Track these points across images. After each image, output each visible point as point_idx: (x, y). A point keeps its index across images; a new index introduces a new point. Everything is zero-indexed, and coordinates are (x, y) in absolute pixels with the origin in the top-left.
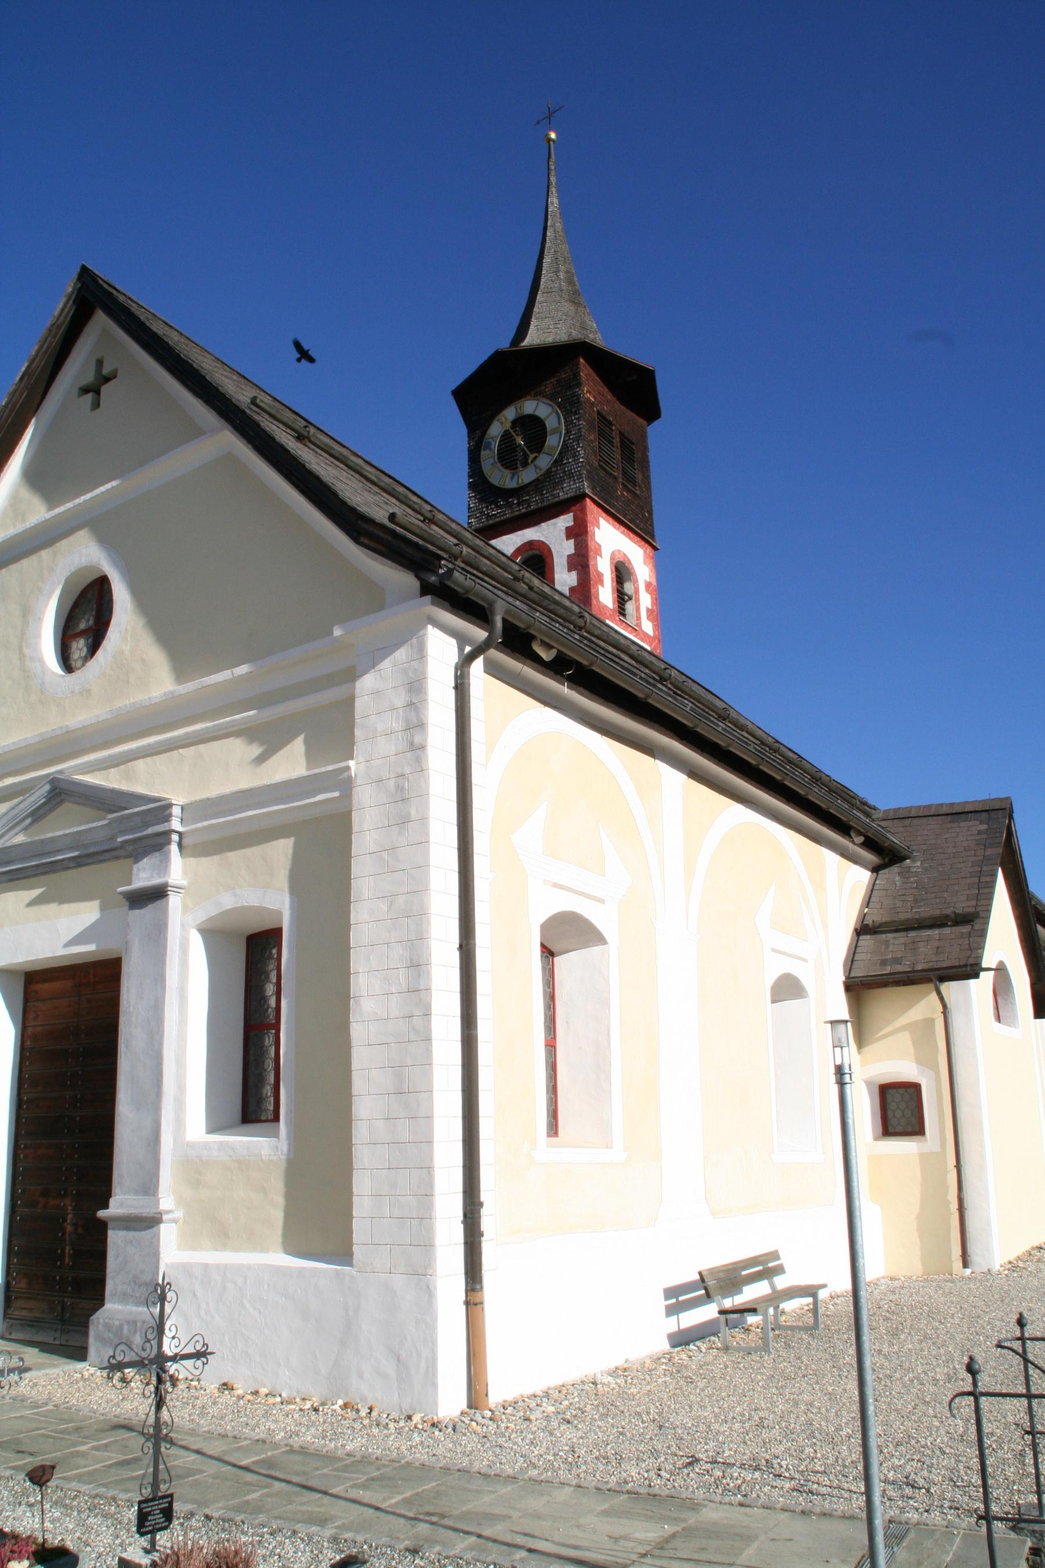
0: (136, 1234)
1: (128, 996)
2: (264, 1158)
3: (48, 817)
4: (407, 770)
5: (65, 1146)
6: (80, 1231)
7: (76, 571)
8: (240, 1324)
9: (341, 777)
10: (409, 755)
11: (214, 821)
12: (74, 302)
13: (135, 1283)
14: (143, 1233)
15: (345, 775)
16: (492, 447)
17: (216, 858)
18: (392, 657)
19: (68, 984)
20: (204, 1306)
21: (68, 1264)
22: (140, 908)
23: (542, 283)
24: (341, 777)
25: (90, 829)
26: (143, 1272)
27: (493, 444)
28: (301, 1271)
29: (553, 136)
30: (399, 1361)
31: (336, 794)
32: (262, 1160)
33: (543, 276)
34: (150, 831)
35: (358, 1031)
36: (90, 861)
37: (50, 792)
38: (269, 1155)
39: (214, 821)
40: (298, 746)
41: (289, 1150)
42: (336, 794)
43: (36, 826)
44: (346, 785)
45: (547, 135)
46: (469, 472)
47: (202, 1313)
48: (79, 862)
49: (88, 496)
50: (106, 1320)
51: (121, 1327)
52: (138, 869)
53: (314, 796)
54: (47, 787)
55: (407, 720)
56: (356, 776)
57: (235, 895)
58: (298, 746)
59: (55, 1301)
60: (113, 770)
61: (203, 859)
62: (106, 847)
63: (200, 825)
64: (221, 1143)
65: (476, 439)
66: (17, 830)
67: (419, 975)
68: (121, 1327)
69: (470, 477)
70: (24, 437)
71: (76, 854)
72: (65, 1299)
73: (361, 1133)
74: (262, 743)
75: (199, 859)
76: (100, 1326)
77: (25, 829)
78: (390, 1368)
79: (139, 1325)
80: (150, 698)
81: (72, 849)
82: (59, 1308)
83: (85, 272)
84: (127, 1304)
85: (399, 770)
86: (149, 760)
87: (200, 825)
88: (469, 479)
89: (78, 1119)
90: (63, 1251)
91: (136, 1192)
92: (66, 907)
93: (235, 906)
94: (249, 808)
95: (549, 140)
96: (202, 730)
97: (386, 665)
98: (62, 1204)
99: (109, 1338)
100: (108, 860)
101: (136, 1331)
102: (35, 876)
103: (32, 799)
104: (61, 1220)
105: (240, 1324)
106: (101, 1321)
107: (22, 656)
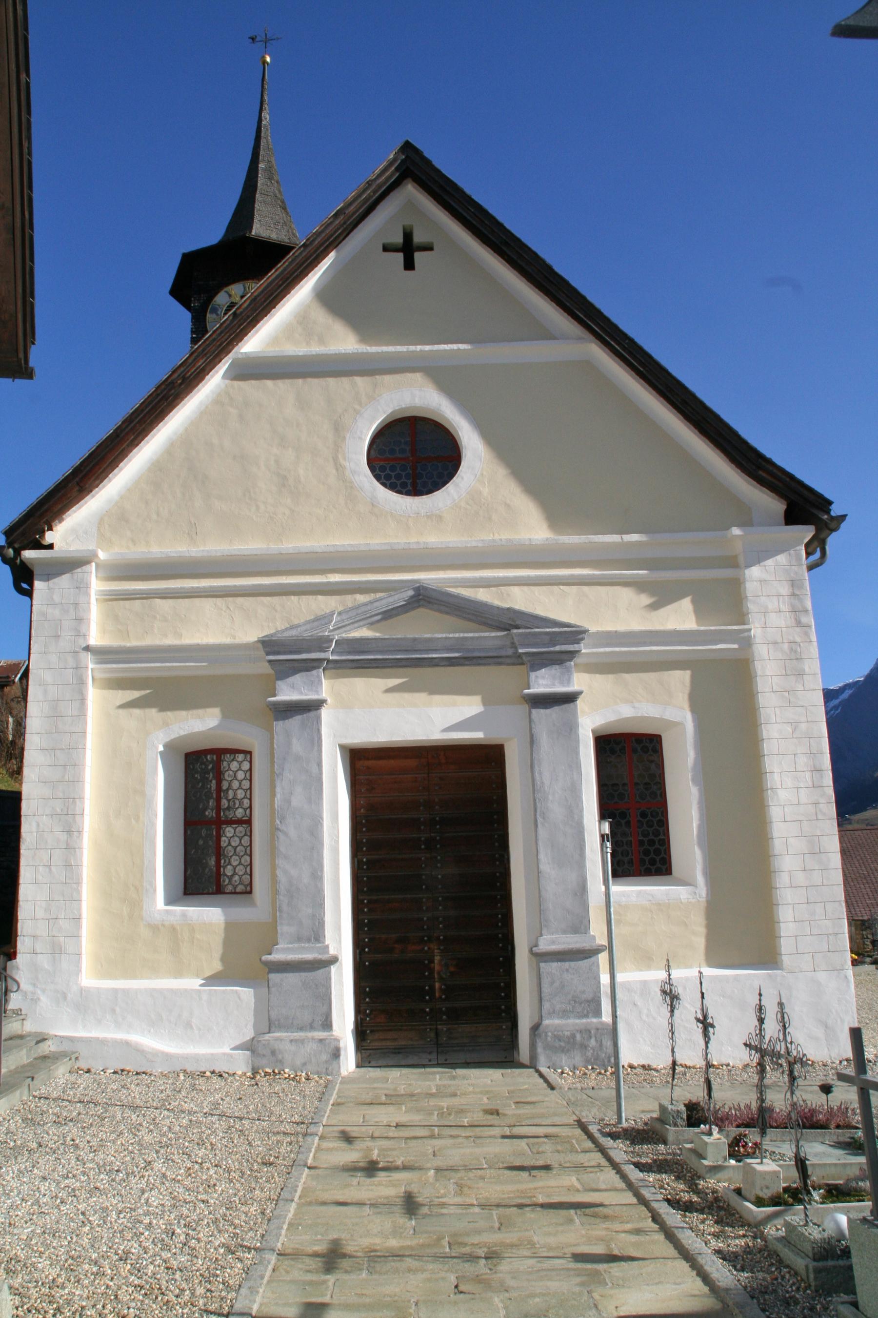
0: (572, 964)
1: (541, 778)
2: (683, 901)
3: (399, 617)
4: (798, 639)
5: (424, 900)
6: (452, 969)
7: (405, 408)
8: (682, 1020)
9: (742, 635)
10: (798, 629)
11: (617, 649)
12: (397, 169)
13: (575, 1002)
14: (580, 962)
15: (746, 634)
16: (219, 312)
17: (611, 677)
18: (774, 559)
19: (412, 763)
20: (645, 1011)
21: (441, 997)
22: (546, 708)
23: (259, 185)
24: (742, 635)
25: (478, 638)
26: (583, 992)
27: (220, 310)
28: (736, 978)
29: (268, 59)
30: (826, 1027)
31: (736, 646)
32: (681, 903)
33: (259, 179)
34: (558, 648)
35: (775, 813)
36: (467, 663)
37: (412, 597)
38: (688, 899)
39: (617, 649)
40: (686, 604)
41: (707, 894)
42: (736, 646)
43: (384, 623)
44: (747, 642)
45: (264, 57)
46: (192, 328)
47: (644, 1017)
48: (451, 662)
49: (427, 348)
50: (555, 1033)
51: (573, 1036)
52: (537, 677)
53: (716, 645)
54: (411, 593)
55: (792, 606)
56: (754, 636)
57: (634, 707)
58: (686, 604)
59: (426, 1029)
60: (481, 589)
61: (597, 675)
62: (495, 654)
63: (602, 650)
64: (640, 892)
65: (202, 301)
66: (361, 623)
67: (822, 777)
68: (573, 1036)
69: (192, 332)
70: (319, 266)
71: (456, 655)
72: (439, 1027)
73: (782, 881)
74: (652, 594)
75: (593, 675)
76: (549, 1039)
77: (372, 624)
78: (820, 1032)
79: (592, 1032)
80: (530, 539)
81: (457, 651)
82: (432, 1035)
83: (407, 147)
84: (568, 1018)
85: (791, 638)
86: (525, 588)
87: (602, 650)
88: (192, 334)
89: (440, 876)
90: (432, 988)
91: (564, 932)
92: (437, 698)
93: (634, 715)
94: (652, 644)
95: (264, 62)
96: (588, 575)
97: (770, 562)
98: (426, 948)
99: (561, 1046)
100: (489, 664)
101: (591, 1037)
102: (391, 667)
103: (391, 600)
104: (426, 962)
105: (682, 1020)
106: (550, 1034)
107: (339, 467)
